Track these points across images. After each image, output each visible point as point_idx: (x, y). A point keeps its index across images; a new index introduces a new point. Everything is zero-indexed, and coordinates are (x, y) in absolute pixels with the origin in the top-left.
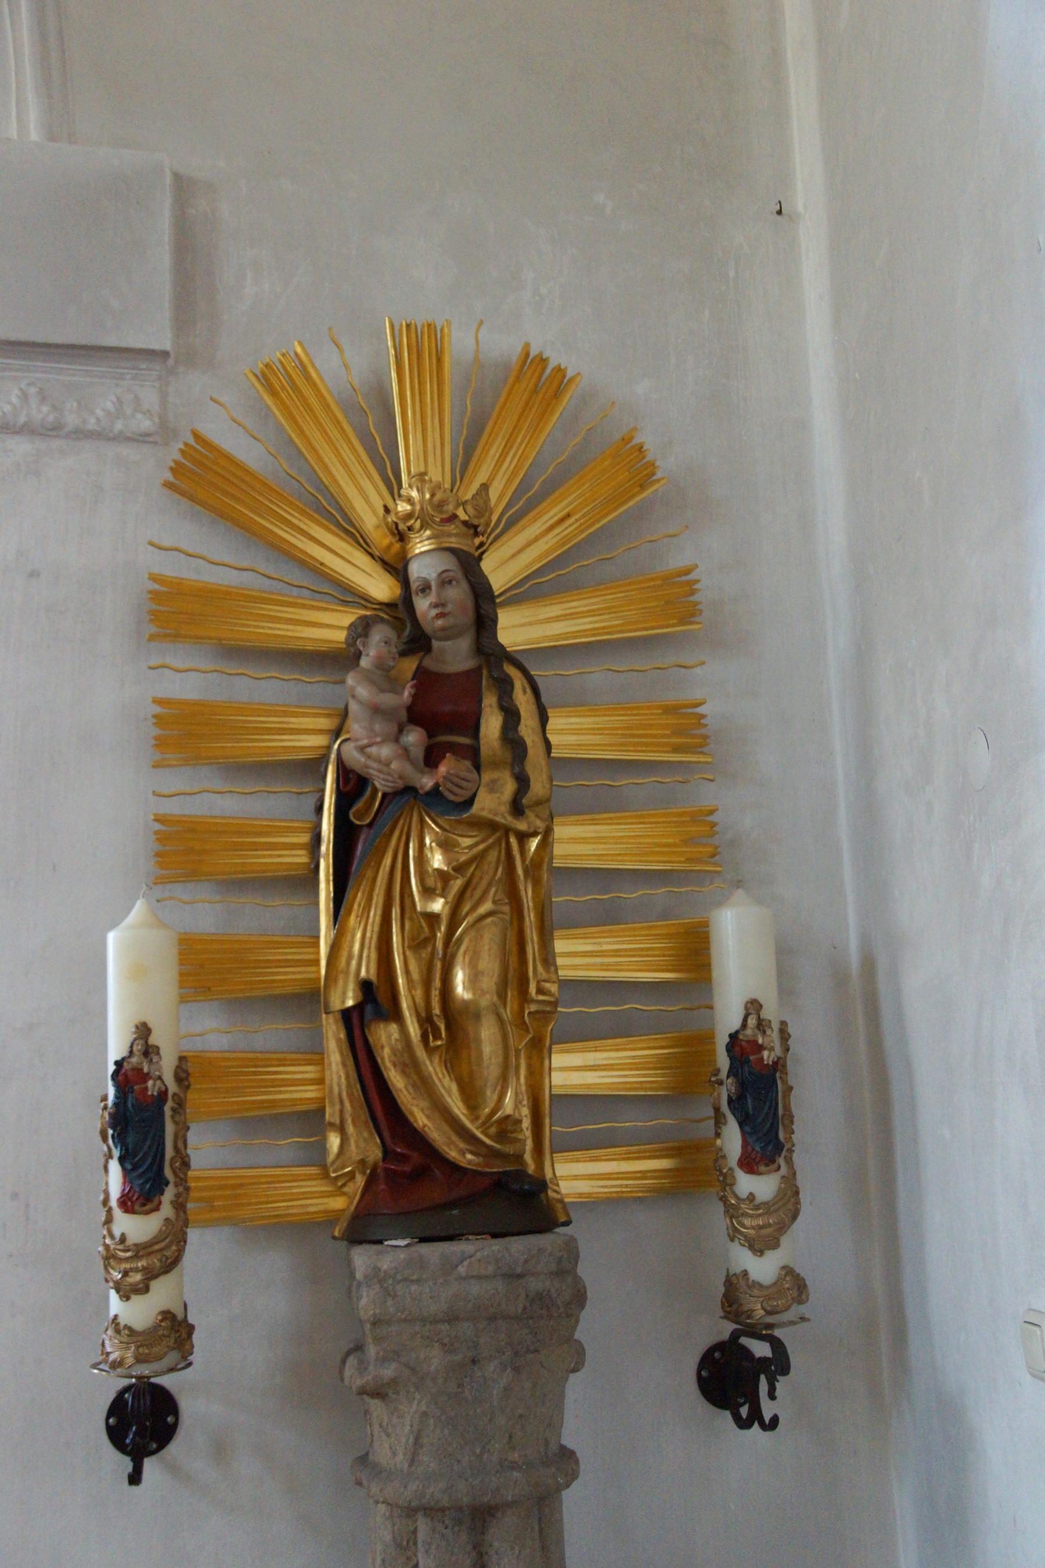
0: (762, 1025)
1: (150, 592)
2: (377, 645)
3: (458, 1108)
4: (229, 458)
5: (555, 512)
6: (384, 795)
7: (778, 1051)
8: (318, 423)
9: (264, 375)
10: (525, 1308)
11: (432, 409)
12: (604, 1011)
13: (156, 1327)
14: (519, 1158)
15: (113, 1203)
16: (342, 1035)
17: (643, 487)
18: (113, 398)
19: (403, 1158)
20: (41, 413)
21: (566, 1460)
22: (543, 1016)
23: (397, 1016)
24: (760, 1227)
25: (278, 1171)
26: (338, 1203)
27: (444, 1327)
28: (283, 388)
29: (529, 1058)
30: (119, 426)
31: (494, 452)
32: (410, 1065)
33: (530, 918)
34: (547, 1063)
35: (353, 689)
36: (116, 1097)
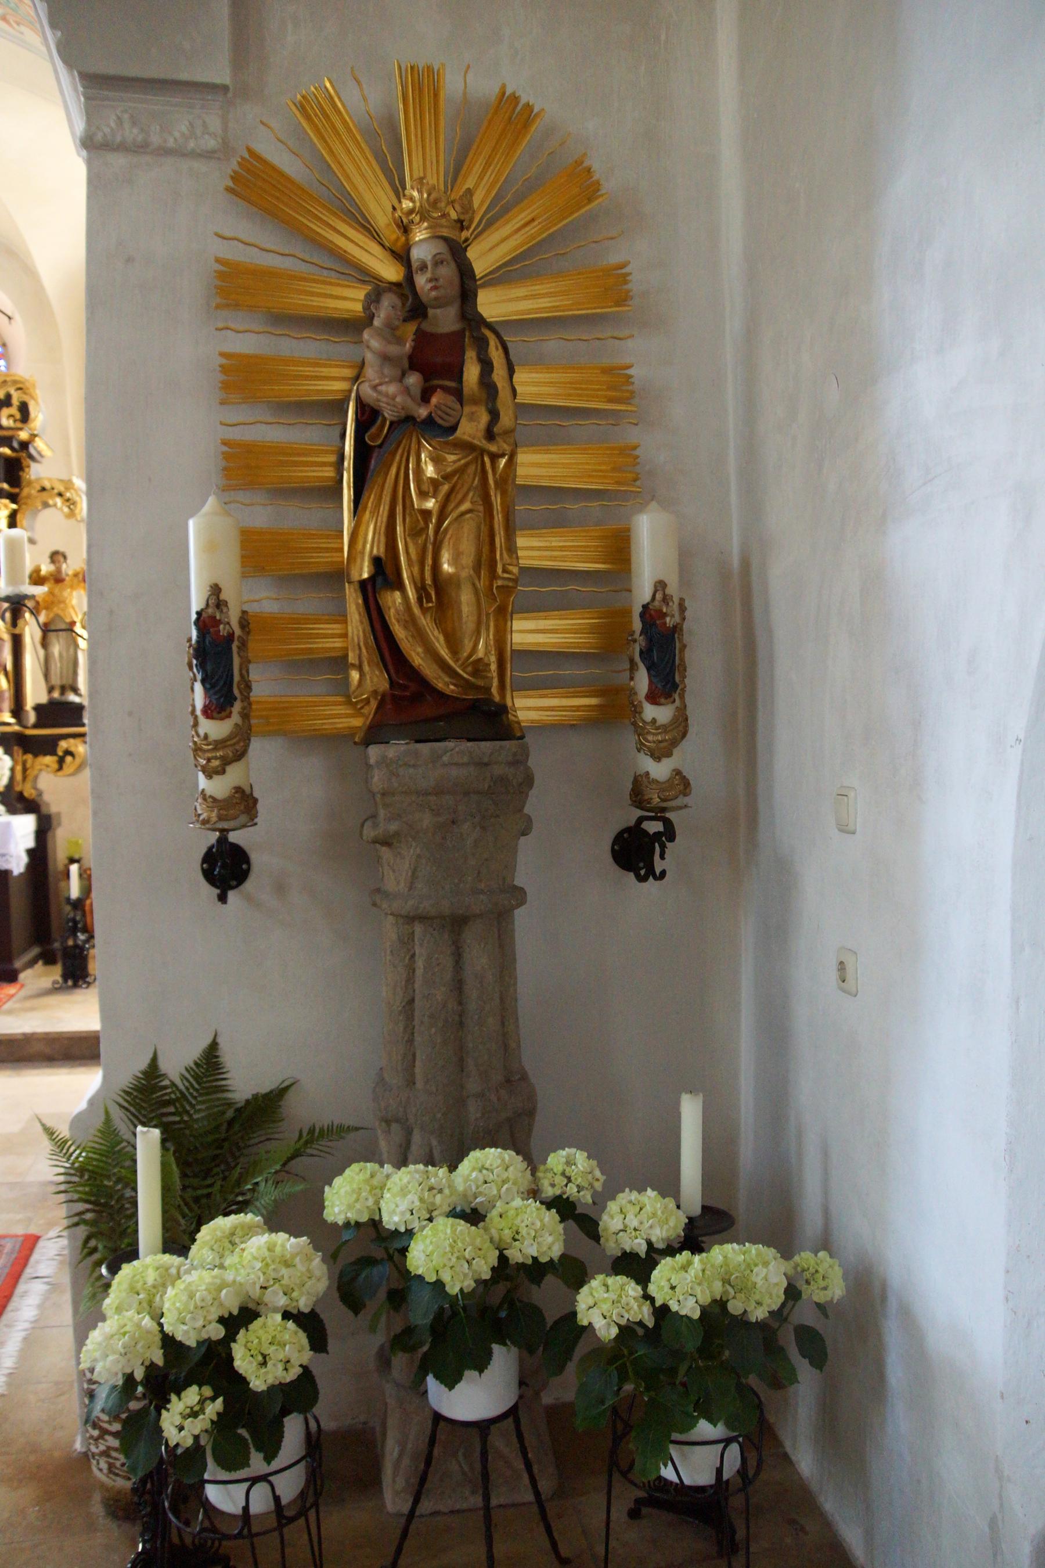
0: (666, 599)
1: (215, 271)
2: (387, 309)
3: (444, 653)
4: (275, 169)
5: (523, 217)
6: (392, 423)
7: (677, 619)
8: (342, 142)
9: (301, 103)
10: (490, 787)
11: (430, 132)
12: (552, 588)
13: (231, 797)
14: (488, 690)
15: (198, 712)
16: (360, 601)
17: (590, 200)
18: (187, 123)
19: (405, 688)
20: (131, 134)
21: (519, 896)
22: (506, 590)
23: (400, 586)
24: (660, 742)
25: (315, 699)
26: (357, 722)
27: (432, 798)
28: (316, 115)
29: (496, 620)
30: (192, 144)
31: (477, 169)
32: (410, 622)
33: (498, 518)
34: (509, 623)
35: (368, 341)
36: (198, 637)
